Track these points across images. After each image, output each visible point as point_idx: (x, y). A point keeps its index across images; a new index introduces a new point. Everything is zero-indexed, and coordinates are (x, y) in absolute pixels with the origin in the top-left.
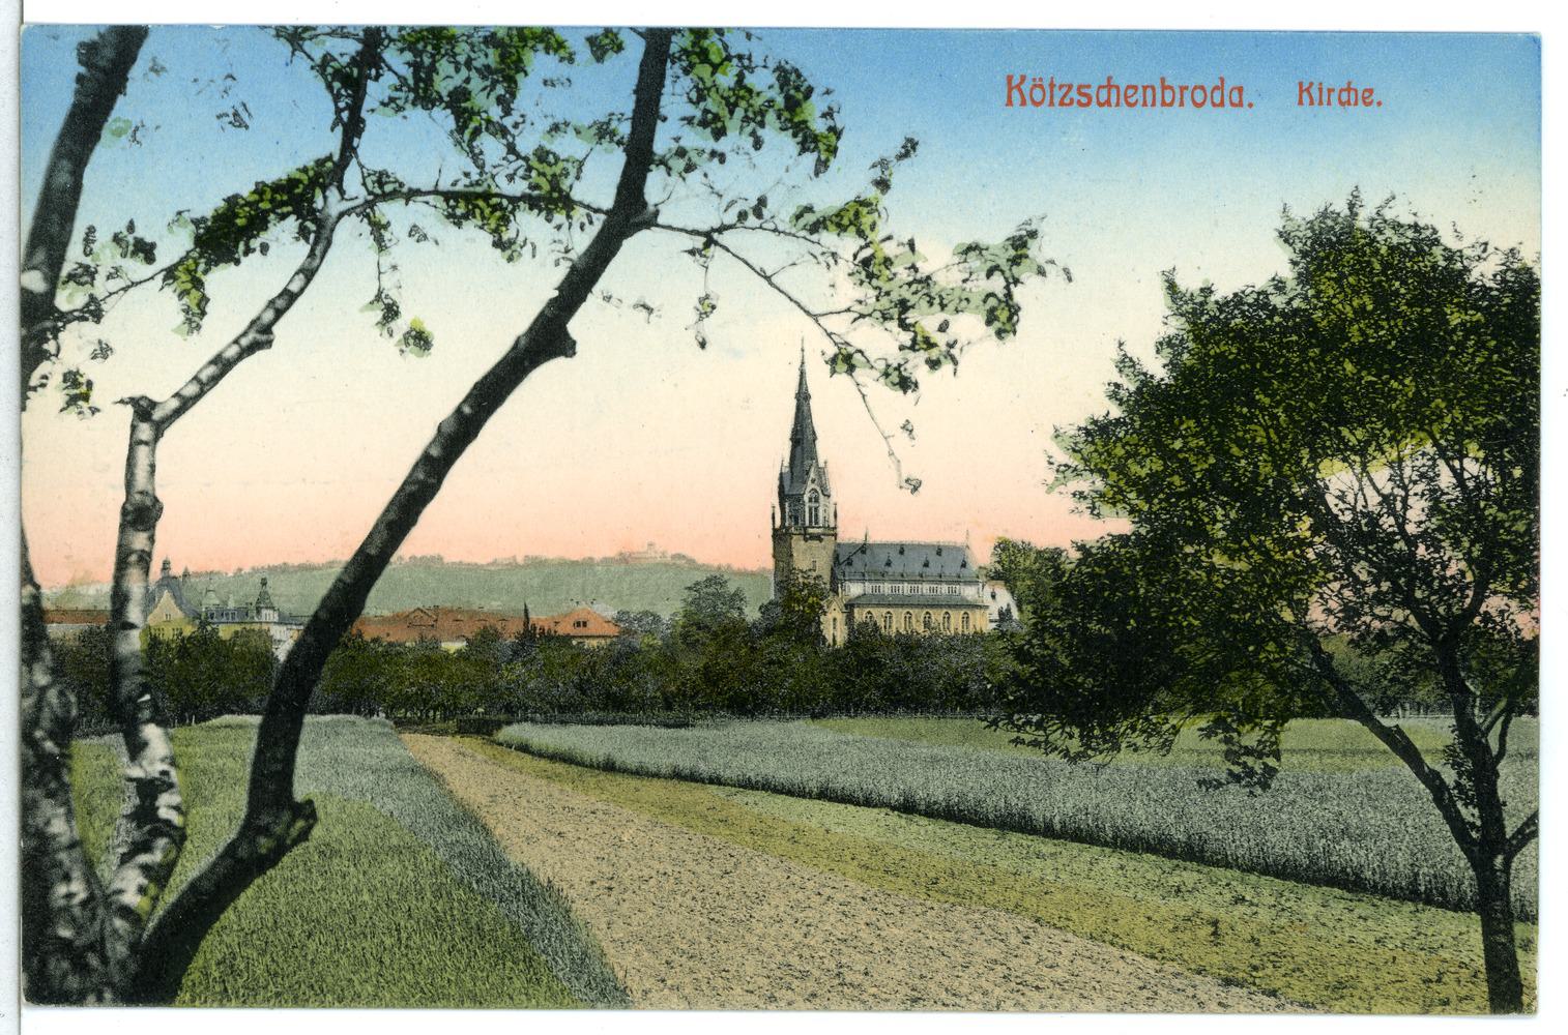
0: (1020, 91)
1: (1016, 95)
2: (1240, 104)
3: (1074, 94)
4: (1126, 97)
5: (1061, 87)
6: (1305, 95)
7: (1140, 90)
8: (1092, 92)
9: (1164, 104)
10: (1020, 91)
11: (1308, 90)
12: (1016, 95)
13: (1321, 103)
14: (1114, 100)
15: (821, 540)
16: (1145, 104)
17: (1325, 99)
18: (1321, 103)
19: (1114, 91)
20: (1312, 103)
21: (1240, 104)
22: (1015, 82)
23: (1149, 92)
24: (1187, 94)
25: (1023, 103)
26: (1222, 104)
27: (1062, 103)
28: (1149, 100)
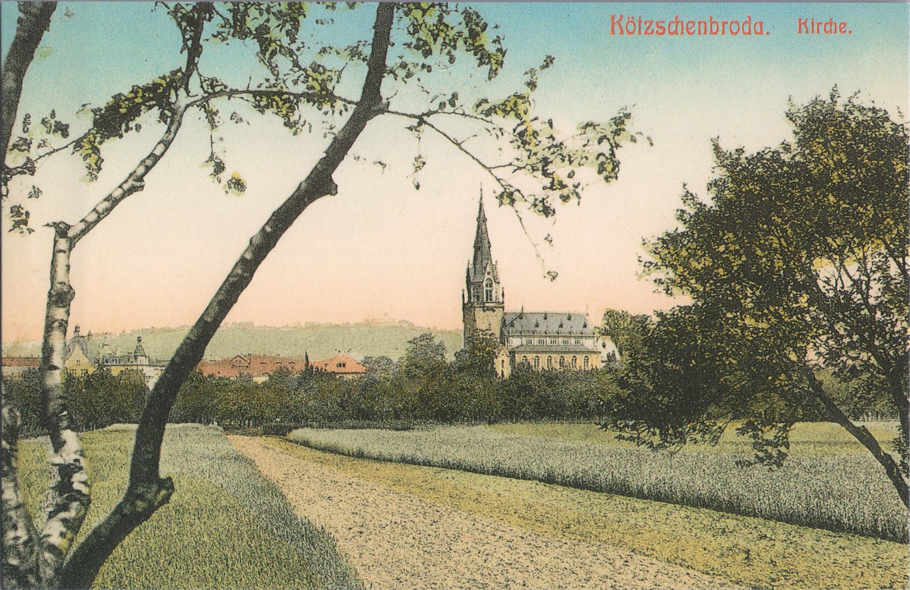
0: (620, 25)
1: (617, 27)
2: (761, 33)
3: (654, 27)
4: (687, 29)
5: (645, 23)
6: (803, 26)
7: (697, 24)
8: (666, 26)
9: (711, 33)
10: (620, 25)
11: (805, 23)
12: (617, 27)
13: (813, 31)
14: (679, 31)
15: (494, 311)
16: (700, 33)
17: (815, 28)
18: (813, 31)
19: (680, 25)
20: (807, 32)
21: (761, 33)
22: (616, 19)
23: (702, 25)
24: (727, 27)
25: (622, 33)
26: (749, 33)
27: (646, 33)
28: (703, 31)
